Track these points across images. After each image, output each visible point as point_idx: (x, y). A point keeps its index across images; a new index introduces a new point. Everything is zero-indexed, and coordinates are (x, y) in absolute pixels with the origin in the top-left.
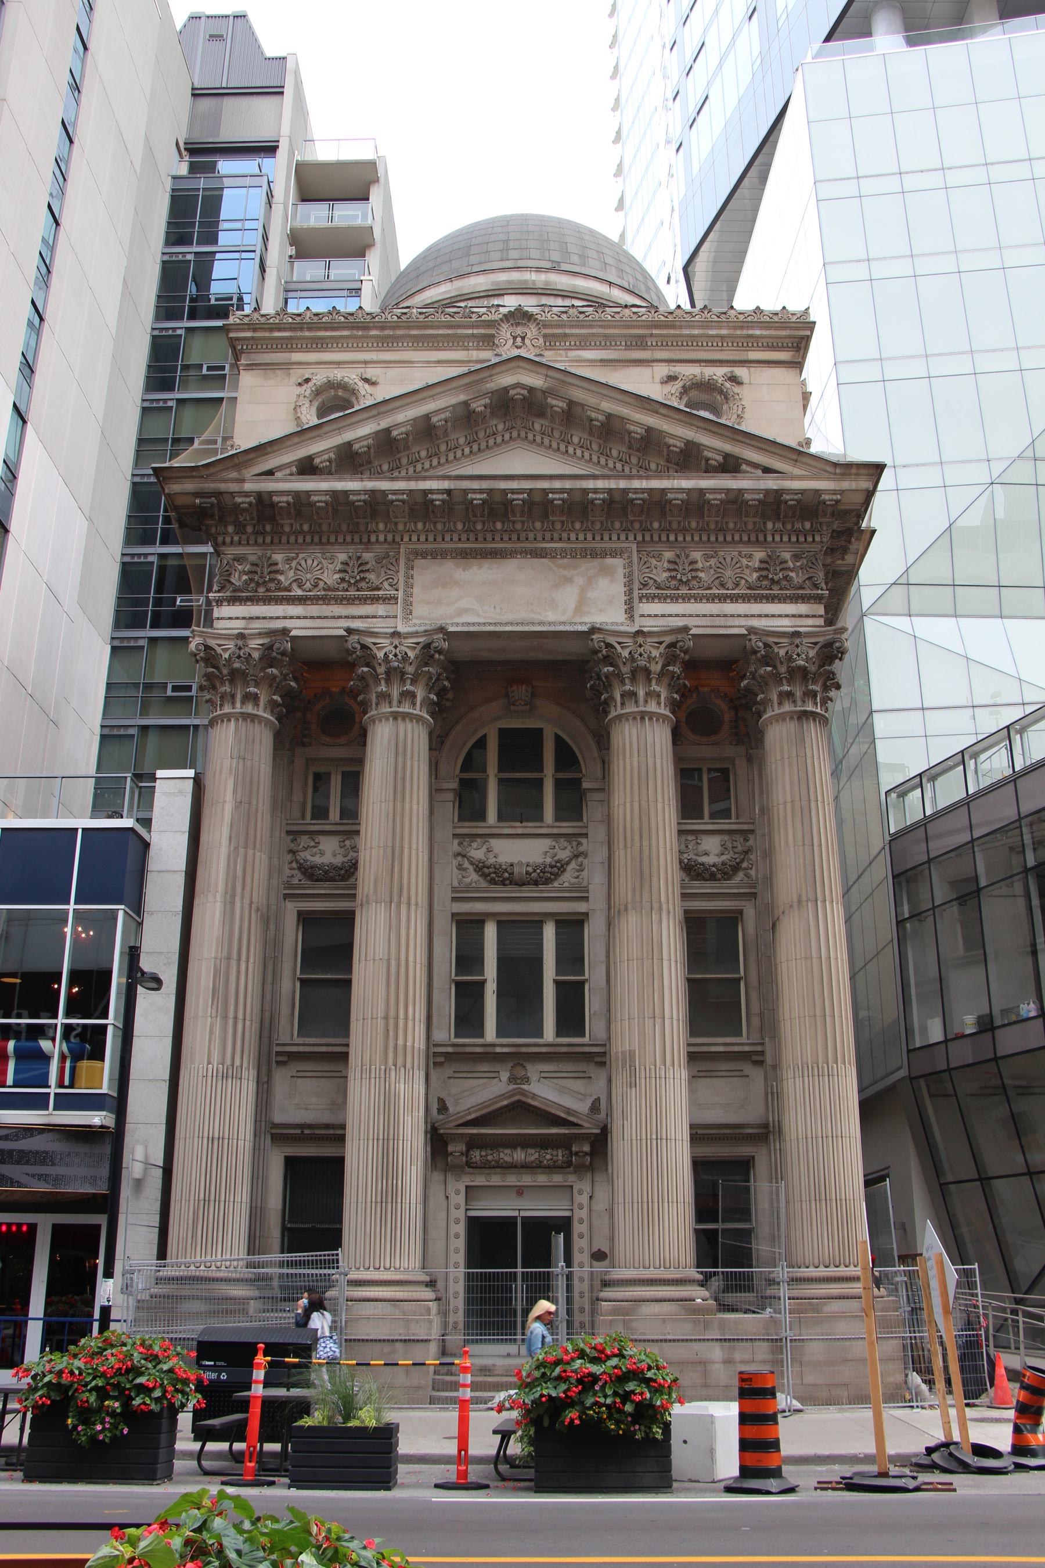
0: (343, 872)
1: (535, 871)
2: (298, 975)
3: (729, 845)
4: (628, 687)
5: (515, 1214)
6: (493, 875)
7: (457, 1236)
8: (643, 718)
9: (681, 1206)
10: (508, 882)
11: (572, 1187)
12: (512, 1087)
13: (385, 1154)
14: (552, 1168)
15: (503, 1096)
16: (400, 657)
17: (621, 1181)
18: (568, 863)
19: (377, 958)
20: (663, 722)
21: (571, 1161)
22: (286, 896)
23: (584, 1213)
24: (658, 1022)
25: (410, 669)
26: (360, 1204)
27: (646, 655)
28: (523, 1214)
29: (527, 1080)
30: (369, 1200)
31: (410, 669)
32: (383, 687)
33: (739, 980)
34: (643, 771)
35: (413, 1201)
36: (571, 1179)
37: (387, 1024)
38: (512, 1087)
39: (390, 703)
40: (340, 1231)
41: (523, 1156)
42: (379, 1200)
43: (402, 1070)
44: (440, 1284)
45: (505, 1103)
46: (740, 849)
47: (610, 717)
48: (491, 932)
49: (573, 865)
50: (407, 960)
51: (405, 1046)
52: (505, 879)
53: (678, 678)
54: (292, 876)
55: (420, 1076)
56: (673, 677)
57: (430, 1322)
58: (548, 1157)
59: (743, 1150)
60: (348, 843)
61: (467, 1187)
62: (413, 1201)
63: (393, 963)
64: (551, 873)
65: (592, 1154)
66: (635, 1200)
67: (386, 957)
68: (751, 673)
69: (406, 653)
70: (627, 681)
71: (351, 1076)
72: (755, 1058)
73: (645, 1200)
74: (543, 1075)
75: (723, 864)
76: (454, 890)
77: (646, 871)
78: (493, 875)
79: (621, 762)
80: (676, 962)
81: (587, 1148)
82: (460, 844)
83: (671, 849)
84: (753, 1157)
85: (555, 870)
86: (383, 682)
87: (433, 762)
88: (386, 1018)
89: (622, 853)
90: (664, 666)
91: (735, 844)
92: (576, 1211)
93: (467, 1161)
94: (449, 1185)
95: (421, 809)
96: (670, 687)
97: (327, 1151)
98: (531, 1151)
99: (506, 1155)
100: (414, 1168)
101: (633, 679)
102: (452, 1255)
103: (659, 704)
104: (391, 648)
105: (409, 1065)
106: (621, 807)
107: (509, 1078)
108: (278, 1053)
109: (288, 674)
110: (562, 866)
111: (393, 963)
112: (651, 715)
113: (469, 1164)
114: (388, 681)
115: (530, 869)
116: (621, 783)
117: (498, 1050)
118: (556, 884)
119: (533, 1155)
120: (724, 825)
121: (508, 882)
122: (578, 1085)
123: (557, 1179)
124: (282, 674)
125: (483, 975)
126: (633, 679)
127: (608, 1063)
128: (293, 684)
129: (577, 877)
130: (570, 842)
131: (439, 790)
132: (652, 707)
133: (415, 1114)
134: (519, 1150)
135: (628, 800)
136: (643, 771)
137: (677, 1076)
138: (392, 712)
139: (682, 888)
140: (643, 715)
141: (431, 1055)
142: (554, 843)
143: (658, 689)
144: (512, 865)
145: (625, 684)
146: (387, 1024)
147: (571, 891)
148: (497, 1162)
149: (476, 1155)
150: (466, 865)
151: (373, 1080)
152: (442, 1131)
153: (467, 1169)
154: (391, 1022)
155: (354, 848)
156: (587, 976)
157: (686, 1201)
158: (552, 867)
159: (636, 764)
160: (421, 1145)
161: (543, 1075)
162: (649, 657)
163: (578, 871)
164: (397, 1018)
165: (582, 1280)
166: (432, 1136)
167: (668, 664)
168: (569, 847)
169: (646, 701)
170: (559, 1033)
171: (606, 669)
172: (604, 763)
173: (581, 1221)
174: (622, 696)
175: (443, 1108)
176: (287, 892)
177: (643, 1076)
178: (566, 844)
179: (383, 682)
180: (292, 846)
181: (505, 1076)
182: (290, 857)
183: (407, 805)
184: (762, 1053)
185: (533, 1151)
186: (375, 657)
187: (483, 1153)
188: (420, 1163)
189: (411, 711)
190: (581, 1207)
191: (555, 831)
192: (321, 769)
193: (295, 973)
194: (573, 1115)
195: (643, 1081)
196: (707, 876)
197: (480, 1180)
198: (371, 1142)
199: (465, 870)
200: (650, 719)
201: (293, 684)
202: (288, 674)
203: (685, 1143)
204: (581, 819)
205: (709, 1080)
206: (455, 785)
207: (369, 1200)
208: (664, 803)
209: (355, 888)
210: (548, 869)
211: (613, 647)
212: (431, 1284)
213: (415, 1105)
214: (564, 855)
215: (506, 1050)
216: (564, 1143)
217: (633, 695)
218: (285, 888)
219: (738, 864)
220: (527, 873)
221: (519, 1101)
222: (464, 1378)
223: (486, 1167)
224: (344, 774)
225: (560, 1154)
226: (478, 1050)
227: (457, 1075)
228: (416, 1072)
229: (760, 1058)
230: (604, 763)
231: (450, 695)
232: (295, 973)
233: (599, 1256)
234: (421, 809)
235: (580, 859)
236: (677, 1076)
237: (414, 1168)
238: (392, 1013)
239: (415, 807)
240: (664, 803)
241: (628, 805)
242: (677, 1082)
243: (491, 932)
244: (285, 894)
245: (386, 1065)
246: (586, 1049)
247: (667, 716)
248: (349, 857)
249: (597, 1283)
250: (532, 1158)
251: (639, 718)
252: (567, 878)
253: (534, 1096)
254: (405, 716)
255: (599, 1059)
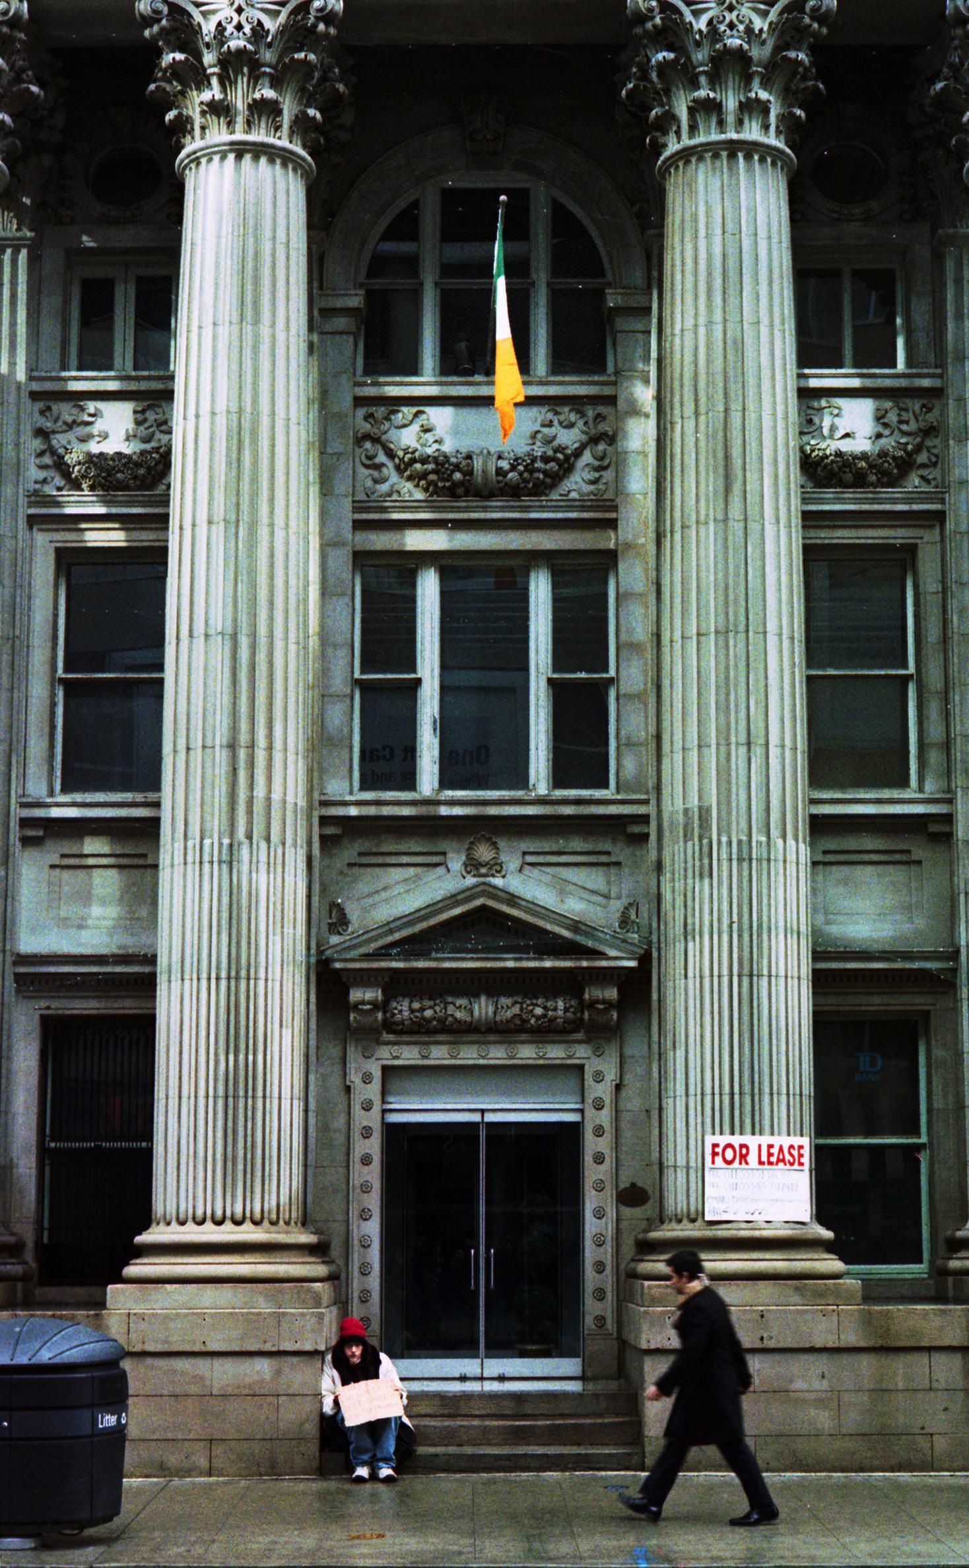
0: (142, 471)
1: (513, 468)
2: (60, 672)
3: (892, 417)
4: (702, 93)
5: (476, 1118)
6: (433, 477)
7: (366, 1160)
8: (732, 156)
9: (795, 1102)
10: (460, 491)
11: (581, 1068)
12: (470, 881)
13: (233, 1008)
14: (545, 1032)
15: (453, 900)
16: (247, 29)
17: (680, 1053)
18: (578, 453)
19: (212, 631)
20: (774, 164)
21: (582, 1019)
22: (32, 521)
23: (604, 1117)
24: (758, 751)
25: (268, 56)
26: (184, 1100)
27: (741, 28)
28: (490, 1118)
29: (496, 867)
30: (202, 1093)
31: (268, 56)
32: (213, 92)
33: (906, 679)
34: (732, 263)
35: (286, 1093)
36: (582, 1052)
37: (234, 759)
38: (470, 881)
39: (229, 124)
40: (148, 1155)
41: (491, 1010)
42: (221, 1092)
43: (263, 845)
44: (336, 1252)
45: (457, 911)
46: (912, 426)
47: (667, 153)
48: (429, 588)
49: (587, 457)
50: (271, 636)
51: (268, 799)
52: (455, 485)
53: (804, 78)
54: (45, 481)
55: (296, 860)
56: (795, 73)
57: (321, 1317)
58: (539, 1011)
59: (917, 1001)
60: (151, 416)
61: (385, 1069)
62: (286, 1093)
63: (244, 641)
64: (545, 472)
65: (621, 1005)
66: (708, 1090)
67: (230, 630)
68: (951, 66)
69: (260, 23)
70: (703, 80)
71: (164, 859)
72: (934, 828)
73: (727, 1089)
74: (529, 859)
75: (883, 454)
76: (358, 507)
77: (737, 462)
78: (433, 477)
79: (689, 247)
80: (792, 638)
81: (612, 994)
82: (369, 417)
83: (786, 418)
84: (927, 1014)
85: (553, 465)
86: (214, 81)
87: (315, 258)
88: (232, 746)
89: (690, 424)
90: (777, 49)
91: (905, 416)
92: (590, 1112)
93: (385, 1021)
94: (352, 1066)
95: (293, 340)
96: (788, 95)
97: (125, 1006)
98: (505, 1001)
99: (459, 1009)
100: (287, 1033)
101: (715, 79)
102: (357, 1169)
103: (766, 127)
104: (230, 12)
105: (275, 838)
106: (689, 336)
107: (466, 865)
108: (25, 823)
109: (23, 70)
110: (567, 458)
111: (244, 641)
112: (750, 149)
113: (389, 1026)
114: (225, 81)
115: (504, 465)
116: (689, 285)
117: (444, 811)
118: (554, 496)
119: (508, 1007)
120: (882, 377)
121: (460, 491)
122: (594, 879)
123: (556, 1053)
124: (12, 67)
125: (413, 669)
126: (715, 79)
127: (653, 837)
128: (34, 89)
129: (594, 482)
130: (582, 414)
131: (327, 313)
132: (752, 132)
133: (289, 930)
134: (483, 999)
135: (702, 320)
136: (732, 263)
137: (792, 857)
138: (232, 143)
139: (804, 501)
140: (733, 148)
141: (316, 821)
142: (550, 416)
143: (764, 95)
144: (469, 457)
145: (696, 86)
146: (234, 759)
147: (583, 509)
148: (442, 1021)
149: (403, 1009)
150: (381, 458)
151: (206, 866)
152: (338, 965)
153: (386, 1037)
154: (242, 754)
155: (165, 426)
156: (612, 672)
157: (805, 1092)
158: (546, 459)
159: (717, 250)
160: (300, 989)
161: (529, 859)
162: (749, 30)
163: (597, 469)
164: (252, 746)
165: (599, 1243)
166: (318, 975)
167: (787, 47)
168: (580, 423)
169: (740, 122)
170: (560, 778)
171: (660, 56)
172: (649, 257)
173: (599, 1131)
174: (691, 111)
175: (340, 921)
176: (32, 511)
177: (724, 856)
178: (573, 417)
179: (214, 81)
180: (42, 422)
181: (456, 863)
182: (37, 444)
183: (265, 331)
184: (948, 818)
185: (509, 1001)
186: (197, 31)
187: (416, 1005)
188: (299, 1023)
189: (271, 140)
190: (599, 1106)
191: (552, 391)
192: (97, 273)
193: (54, 669)
194: (586, 934)
195: (725, 864)
196: (848, 477)
197: (409, 1055)
198: (204, 983)
199: (379, 467)
200: (749, 157)
201: (34, 89)
202: (23, 70)
203: (804, 984)
204: (602, 369)
205: (845, 870)
206: (356, 301)
207: (202, 1093)
208: (772, 325)
209: (166, 503)
210: (539, 464)
211: (676, 10)
212: (319, 1250)
213: (289, 914)
214: (569, 438)
215: (458, 811)
216: (569, 984)
217: (712, 108)
218: (30, 505)
219: (909, 454)
220: (500, 472)
221: (483, 907)
222: (657, 1321)
223: (420, 1031)
224: (140, 281)
225: (561, 1004)
226: (406, 811)
227: (365, 860)
228: (290, 851)
229: (945, 828)
230: (649, 257)
231: (348, 117)
232: (54, 669)
233: (632, 1196)
234: (293, 340)
235: (601, 447)
236: (792, 857)
237: (287, 1033)
238: (244, 738)
239: (281, 336)
240: (772, 325)
241: (702, 331)
242: (792, 868)
243: (429, 588)
244: (30, 517)
245: (232, 835)
246: (613, 810)
247: (782, 152)
248: (153, 444)
249: (628, 1250)
250: (509, 1014)
251: (724, 154)
252: (577, 483)
253: (512, 899)
254: (259, 151)
255: (636, 829)
